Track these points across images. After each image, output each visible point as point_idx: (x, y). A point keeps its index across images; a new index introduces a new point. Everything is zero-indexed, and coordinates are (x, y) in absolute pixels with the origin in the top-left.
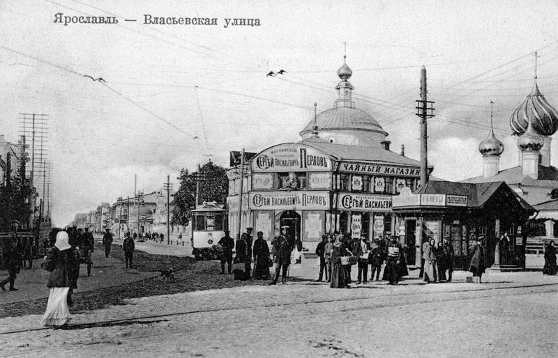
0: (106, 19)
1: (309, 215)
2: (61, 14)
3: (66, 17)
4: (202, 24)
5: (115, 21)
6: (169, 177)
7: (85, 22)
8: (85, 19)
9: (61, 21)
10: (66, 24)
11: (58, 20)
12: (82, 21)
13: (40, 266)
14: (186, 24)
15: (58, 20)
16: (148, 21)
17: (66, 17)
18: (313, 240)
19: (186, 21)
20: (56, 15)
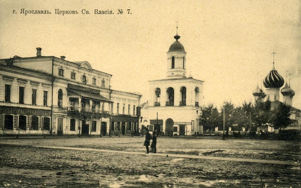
0: (44, 12)
1: (153, 106)
2: (24, 9)
3: (26, 11)
4: (68, 13)
5: (111, 12)
6: (157, 113)
7: (35, 13)
8: (35, 12)
9: (23, 13)
10: (26, 15)
11: (23, 12)
12: (33, 12)
13: (260, 75)
14: (87, 14)
15: (23, 12)
16: (96, 13)
17: (26, 11)
18: (182, 55)
19: (73, 12)
20: (21, 10)
